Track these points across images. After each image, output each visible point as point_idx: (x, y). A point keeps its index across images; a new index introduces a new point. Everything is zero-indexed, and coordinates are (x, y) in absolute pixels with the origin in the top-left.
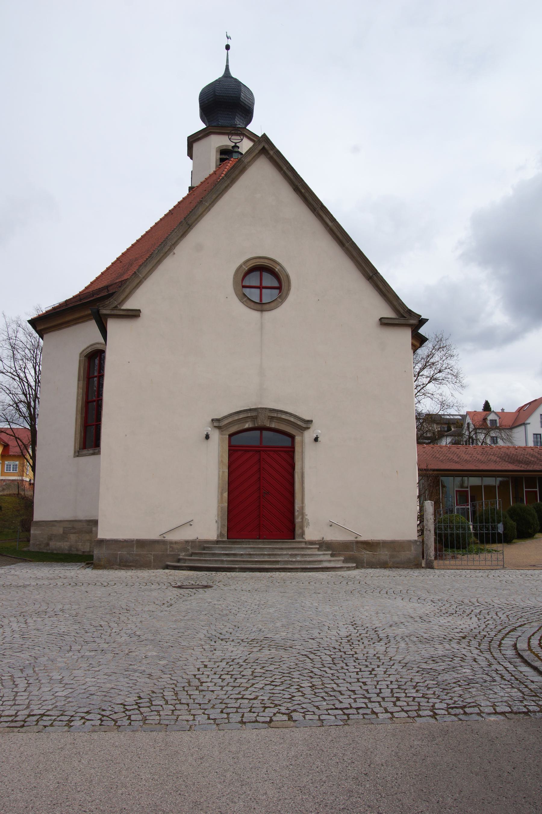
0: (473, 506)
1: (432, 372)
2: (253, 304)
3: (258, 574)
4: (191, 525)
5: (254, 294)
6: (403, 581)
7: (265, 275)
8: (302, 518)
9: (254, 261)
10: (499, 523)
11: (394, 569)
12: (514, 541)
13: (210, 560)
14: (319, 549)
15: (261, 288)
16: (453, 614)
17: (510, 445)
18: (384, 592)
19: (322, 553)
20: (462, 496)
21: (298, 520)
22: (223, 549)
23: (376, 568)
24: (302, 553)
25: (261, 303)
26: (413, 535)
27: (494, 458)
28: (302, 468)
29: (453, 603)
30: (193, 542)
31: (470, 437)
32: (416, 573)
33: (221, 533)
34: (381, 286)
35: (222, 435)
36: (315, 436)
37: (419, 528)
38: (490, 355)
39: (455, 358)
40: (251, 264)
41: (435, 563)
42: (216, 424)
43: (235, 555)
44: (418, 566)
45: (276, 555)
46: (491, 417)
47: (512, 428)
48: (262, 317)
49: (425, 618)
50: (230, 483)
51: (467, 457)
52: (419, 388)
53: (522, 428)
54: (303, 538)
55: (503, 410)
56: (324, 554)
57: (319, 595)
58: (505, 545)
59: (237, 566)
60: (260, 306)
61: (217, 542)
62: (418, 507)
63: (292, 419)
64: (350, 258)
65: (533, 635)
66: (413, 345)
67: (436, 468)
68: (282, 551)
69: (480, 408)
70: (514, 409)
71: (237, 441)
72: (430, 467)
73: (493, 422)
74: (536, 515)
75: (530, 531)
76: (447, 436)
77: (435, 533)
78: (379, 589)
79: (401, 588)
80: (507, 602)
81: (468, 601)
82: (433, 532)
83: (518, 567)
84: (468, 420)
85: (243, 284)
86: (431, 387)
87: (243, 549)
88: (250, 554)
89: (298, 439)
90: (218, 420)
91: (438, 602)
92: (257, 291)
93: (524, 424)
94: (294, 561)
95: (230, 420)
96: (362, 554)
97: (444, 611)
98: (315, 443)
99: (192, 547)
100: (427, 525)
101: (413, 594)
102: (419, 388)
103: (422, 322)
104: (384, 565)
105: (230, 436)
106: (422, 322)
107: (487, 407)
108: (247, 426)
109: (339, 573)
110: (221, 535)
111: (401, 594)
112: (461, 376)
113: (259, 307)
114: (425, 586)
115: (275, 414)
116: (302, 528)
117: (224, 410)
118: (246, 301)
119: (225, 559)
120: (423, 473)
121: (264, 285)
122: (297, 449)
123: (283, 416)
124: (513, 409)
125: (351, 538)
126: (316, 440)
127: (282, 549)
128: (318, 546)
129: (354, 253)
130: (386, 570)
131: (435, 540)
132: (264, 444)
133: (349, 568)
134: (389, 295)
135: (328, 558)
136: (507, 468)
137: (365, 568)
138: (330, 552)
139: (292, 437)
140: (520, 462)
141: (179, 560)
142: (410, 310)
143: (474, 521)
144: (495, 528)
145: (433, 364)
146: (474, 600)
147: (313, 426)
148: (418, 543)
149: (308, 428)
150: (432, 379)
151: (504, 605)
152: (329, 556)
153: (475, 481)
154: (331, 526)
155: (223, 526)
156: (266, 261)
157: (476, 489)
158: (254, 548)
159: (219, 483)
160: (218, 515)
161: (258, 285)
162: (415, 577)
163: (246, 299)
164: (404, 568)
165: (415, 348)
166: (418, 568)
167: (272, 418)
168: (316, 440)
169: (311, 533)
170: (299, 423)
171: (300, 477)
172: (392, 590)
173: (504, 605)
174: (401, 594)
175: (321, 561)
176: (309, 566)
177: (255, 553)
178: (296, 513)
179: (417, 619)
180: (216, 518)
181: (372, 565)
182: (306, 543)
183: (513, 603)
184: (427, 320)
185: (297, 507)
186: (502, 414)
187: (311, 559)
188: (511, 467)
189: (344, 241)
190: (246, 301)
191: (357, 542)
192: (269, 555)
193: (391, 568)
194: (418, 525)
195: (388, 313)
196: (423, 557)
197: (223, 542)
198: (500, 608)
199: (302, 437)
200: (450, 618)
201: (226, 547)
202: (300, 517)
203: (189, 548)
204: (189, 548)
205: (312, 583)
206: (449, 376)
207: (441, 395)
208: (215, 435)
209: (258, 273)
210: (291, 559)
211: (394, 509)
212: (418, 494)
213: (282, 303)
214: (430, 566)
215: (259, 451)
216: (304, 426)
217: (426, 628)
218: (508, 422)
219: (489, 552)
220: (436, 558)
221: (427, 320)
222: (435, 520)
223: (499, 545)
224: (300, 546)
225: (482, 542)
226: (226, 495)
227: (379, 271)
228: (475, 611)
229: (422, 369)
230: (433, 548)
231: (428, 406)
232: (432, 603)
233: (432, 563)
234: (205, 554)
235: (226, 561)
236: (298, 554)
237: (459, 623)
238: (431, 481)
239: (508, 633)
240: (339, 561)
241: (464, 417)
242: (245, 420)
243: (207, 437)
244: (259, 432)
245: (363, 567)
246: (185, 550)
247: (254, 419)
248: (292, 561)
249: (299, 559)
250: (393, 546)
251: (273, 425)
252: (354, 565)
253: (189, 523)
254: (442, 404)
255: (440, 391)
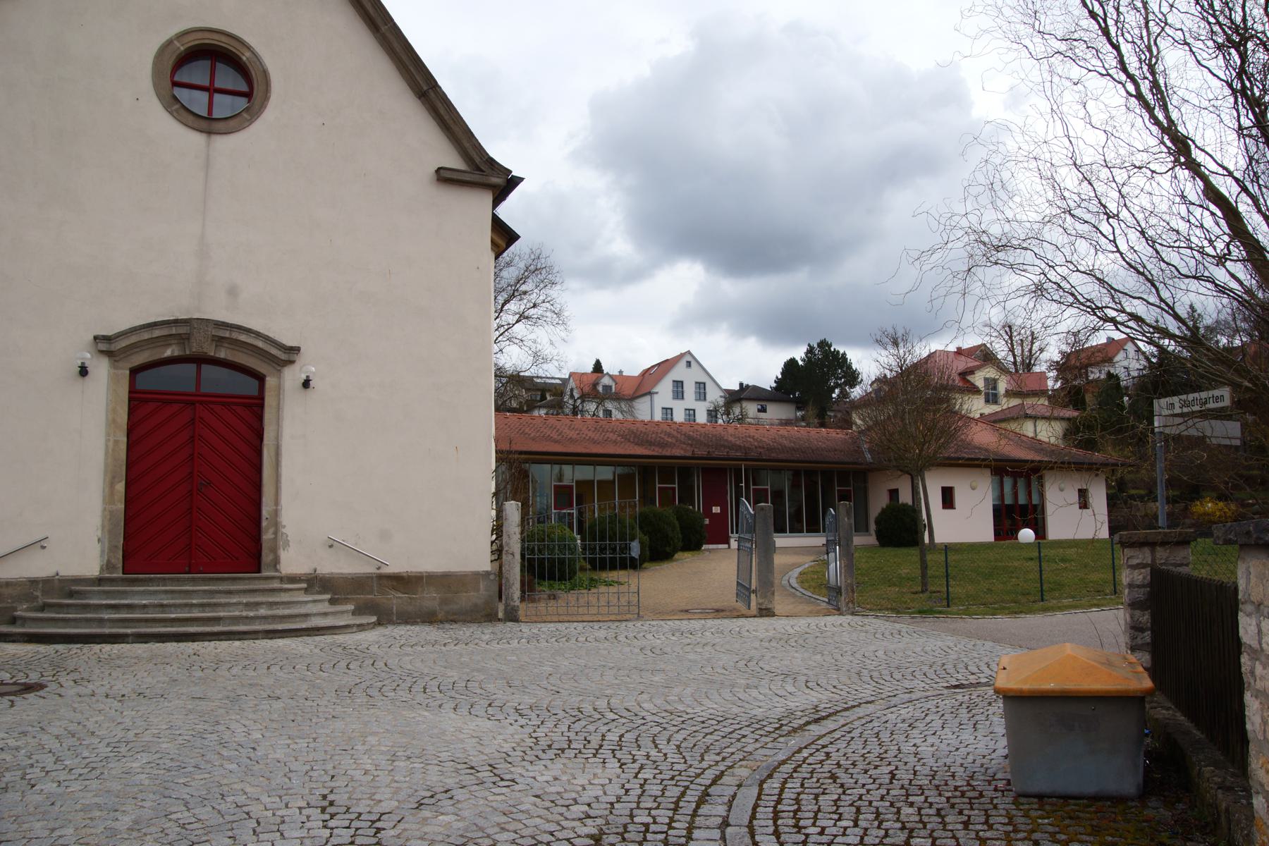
0: (580, 513)
1: (523, 307)
2: (191, 118)
3: (171, 647)
4: (43, 547)
5: (197, 101)
6: (461, 655)
7: (220, 67)
8: (276, 533)
9: (200, 35)
10: (632, 539)
11: (447, 626)
12: (645, 565)
13: (75, 620)
14: (306, 590)
15: (211, 90)
16: (563, 750)
17: (630, 418)
18: (418, 688)
19: (310, 598)
20: (563, 495)
21: (267, 536)
22: (108, 594)
23: (414, 623)
24: (271, 600)
25: (210, 118)
26: (482, 561)
27: (613, 437)
28: (278, 438)
29: (561, 714)
30: (47, 582)
31: (575, 407)
32: (485, 633)
33: (109, 561)
34: (442, 111)
35: (115, 368)
36: (304, 377)
37: (495, 547)
38: (602, 299)
39: (558, 287)
40: (192, 41)
41: (523, 609)
42: (103, 346)
43: (130, 607)
44: (491, 617)
45: (216, 605)
46: (606, 381)
47: (633, 398)
48: (208, 145)
49: (502, 767)
50: (130, 465)
51: (573, 434)
52: (502, 330)
53: (648, 398)
54: (277, 570)
55: (621, 372)
56: (315, 601)
57: (278, 705)
58: (631, 572)
59: (129, 631)
60: (208, 124)
61: (100, 581)
62: (494, 513)
63: (260, 344)
64: (389, 54)
65: (753, 817)
66: (493, 241)
67: (525, 449)
68: (230, 597)
69: (590, 369)
70: (636, 372)
71: (148, 381)
72: (514, 448)
73: (607, 388)
74: (677, 523)
75: (668, 549)
76: (540, 407)
77: (523, 556)
78: (409, 679)
79: (454, 675)
80: (669, 708)
81: (591, 708)
82: (518, 557)
83: (662, 613)
84: (572, 384)
85: (177, 78)
86: (520, 329)
87: (152, 595)
88: (162, 606)
89: (270, 381)
90: (107, 339)
91: (529, 712)
92: (204, 96)
93: (650, 393)
94: (252, 618)
95: (133, 339)
96: (388, 598)
97: (544, 743)
98: (303, 390)
99: (45, 593)
100: (508, 544)
101: (479, 691)
102: (502, 330)
103: (512, 182)
104: (429, 618)
105: (134, 372)
106: (512, 182)
107: (598, 367)
108: (168, 353)
109: (340, 638)
110: (109, 566)
111: (453, 694)
112: (566, 314)
113: (204, 124)
114: (504, 667)
115: (224, 332)
116: (275, 550)
117: (123, 317)
118: (176, 111)
119: (106, 617)
120: (503, 457)
121: (218, 84)
122: (269, 401)
123: (243, 338)
124: (634, 370)
125: (370, 569)
126: (306, 384)
127: (230, 592)
128: (305, 585)
129: (396, 45)
130: (431, 628)
131: (522, 566)
132: (203, 390)
133: (361, 627)
134: (456, 129)
135: (325, 607)
136: (632, 452)
137: (394, 623)
138: (329, 596)
139: (261, 379)
140: (651, 444)
141: (13, 621)
142: (492, 159)
143: (580, 531)
144: (626, 548)
145: (525, 293)
146: (602, 704)
147: (301, 360)
148: (492, 577)
149: (292, 362)
150: (522, 317)
151: (664, 714)
152: (327, 604)
153: (584, 473)
154: (331, 546)
155: (112, 548)
156: (223, 39)
157: (585, 486)
158: (172, 592)
159: (106, 465)
160: (103, 527)
161: (206, 83)
162: (484, 645)
163: (177, 106)
164: (465, 622)
165: (498, 251)
166: (490, 621)
167: (220, 341)
168: (306, 384)
169: (293, 561)
170: (274, 351)
171: (273, 454)
172: (435, 683)
173: (664, 714)
174: (453, 694)
175: (306, 616)
176: (280, 627)
177: (172, 602)
178: (264, 524)
179: (485, 774)
180: (99, 533)
181: (407, 618)
182: (281, 579)
183: (681, 708)
184: (521, 179)
185: (266, 511)
186: (619, 378)
187: (287, 612)
188: (639, 451)
189: (379, 21)
190: (176, 111)
191: (381, 577)
192: (202, 605)
193: (442, 622)
194: (492, 542)
195: (453, 161)
196: (500, 598)
197: (112, 581)
198: (659, 724)
199: (279, 378)
200: (559, 764)
201: (114, 592)
202: (272, 530)
203: (38, 594)
204: (38, 594)
205: (273, 669)
206: (549, 314)
207: (535, 342)
208: (101, 369)
209: (206, 64)
210: (244, 614)
211: (452, 518)
212: (493, 490)
213: (251, 122)
214: (512, 616)
215: (194, 401)
216: (283, 356)
217: (504, 807)
218: (628, 391)
219: (608, 584)
220: (522, 599)
221: (521, 179)
222: (522, 533)
223: (622, 572)
224: (271, 586)
225: (594, 568)
226: (121, 487)
227: (440, 83)
228: (609, 736)
229: (506, 302)
230: (517, 585)
231: (514, 358)
232: (517, 717)
233: (516, 611)
234: (68, 606)
235: (110, 620)
236: (262, 603)
237: (582, 780)
238: (515, 471)
239: (695, 814)
240: (343, 612)
241: (565, 381)
242: (165, 340)
243: (83, 371)
244: (193, 367)
245: (391, 622)
246: (30, 598)
247: (183, 339)
248: (247, 617)
249: (263, 612)
250: (446, 582)
251: (222, 354)
252: (374, 619)
253: (41, 544)
254: (536, 355)
255: (533, 336)
